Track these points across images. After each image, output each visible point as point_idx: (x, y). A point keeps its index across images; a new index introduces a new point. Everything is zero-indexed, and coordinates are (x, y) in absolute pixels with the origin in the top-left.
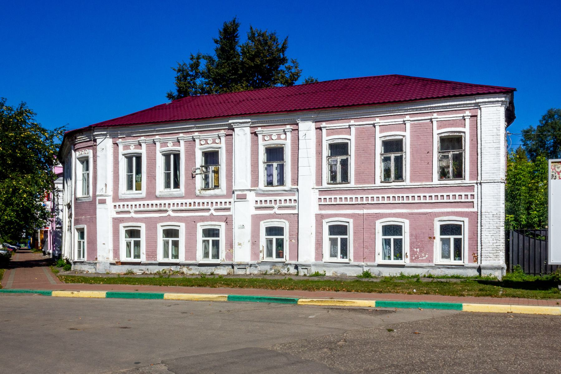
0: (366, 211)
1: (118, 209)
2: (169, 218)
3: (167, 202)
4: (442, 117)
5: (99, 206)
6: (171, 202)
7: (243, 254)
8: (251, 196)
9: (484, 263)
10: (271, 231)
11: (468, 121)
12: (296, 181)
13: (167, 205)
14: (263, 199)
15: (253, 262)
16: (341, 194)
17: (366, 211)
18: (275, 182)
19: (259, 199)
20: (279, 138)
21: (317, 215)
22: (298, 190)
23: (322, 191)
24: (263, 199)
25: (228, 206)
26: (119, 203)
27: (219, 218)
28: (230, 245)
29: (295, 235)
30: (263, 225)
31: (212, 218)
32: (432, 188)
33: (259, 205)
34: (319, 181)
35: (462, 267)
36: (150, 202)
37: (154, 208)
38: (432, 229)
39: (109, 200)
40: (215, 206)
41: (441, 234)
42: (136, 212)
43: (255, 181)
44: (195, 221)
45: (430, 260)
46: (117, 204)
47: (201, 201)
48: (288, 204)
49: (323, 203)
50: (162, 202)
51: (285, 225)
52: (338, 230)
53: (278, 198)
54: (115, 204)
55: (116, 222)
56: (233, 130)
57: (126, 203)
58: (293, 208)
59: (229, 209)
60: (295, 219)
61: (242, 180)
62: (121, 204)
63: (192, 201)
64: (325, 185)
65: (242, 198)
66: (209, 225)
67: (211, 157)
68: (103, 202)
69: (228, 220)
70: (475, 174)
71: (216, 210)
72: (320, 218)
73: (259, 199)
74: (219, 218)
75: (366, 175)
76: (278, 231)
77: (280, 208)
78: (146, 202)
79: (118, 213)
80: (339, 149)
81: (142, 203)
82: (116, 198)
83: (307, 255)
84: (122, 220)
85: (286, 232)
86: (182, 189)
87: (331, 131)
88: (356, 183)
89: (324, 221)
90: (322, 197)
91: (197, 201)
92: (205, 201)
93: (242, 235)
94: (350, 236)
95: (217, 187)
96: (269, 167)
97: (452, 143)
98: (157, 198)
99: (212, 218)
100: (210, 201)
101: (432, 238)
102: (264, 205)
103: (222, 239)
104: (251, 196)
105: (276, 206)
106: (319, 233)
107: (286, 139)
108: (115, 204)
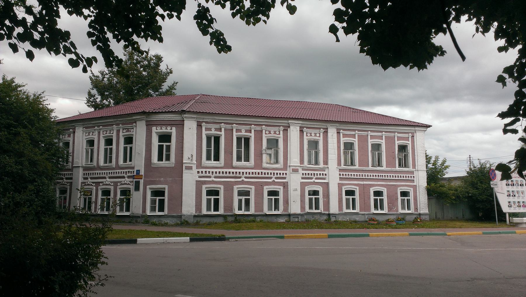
0: (365, 183)
1: (200, 174)
2: (243, 182)
3: (241, 171)
4: (400, 135)
5: (184, 171)
6: (245, 171)
7: (295, 208)
8: (301, 171)
9: (422, 212)
10: (210, 193)
11: (410, 138)
12: (326, 162)
13: (241, 173)
14: (307, 172)
15: (302, 213)
16: (346, 172)
17: (365, 183)
18: (313, 162)
19: (304, 172)
20: (315, 136)
21: (197, 181)
22: (328, 167)
23: (340, 170)
24: (307, 172)
25: (284, 176)
26: (202, 170)
27: (279, 184)
28: (286, 202)
29: (327, 196)
30: (204, 189)
31: (274, 183)
32: (396, 172)
33: (304, 176)
34: (339, 164)
35: (357, 214)
36: (228, 170)
37: (231, 175)
38: (397, 193)
39: (194, 167)
40: (276, 176)
41: (207, 196)
42: (215, 177)
43: (302, 161)
44: (262, 185)
45: (397, 211)
46: (200, 170)
47: (266, 171)
48: (321, 176)
49: (341, 177)
50: (238, 171)
51: (320, 189)
52: (350, 193)
53: (316, 172)
54: (198, 170)
55: (199, 184)
56: (289, 127)
57: (208, 170)
58: (324, 179)
59: (285, 178)
60: (326, 186)
61: (294, 160)
62: (204, 170)
63: (260, 171)
64: (343, 167)
65: (295, 171)
66: (273, 188)
67: (273, 143)
68: (190, 168)
69: (285, 186)
70: (414, 166)
71: (276, 178)
72: (340, 186)
73: (304, 172)
74: (279, 184)
75: (363, 162)
76: (316, 193)
77: (316, 179)
78: (254, 171)
79: (200, 177)
80: (349, 146)
81: (221, 170)
82: (199, 165)
83: (334, 209)
84: (205, 183)
85: (321, 193)
86: (252, 162)
87: (345, 136)
88: (359, 166)
89: (204, 187)
90: (341, 173)
91: (264, 171)
92: (269, 171)
93: (295, 195)
94: (357, 197)
95: (277, 162)
96: (345, 153)
97: (403, 148)
98: (233, 168)
99: (274, 183)
100: (272, 172)
101: (397, 199)
102: (307, 176)
103: (281, 197)
104: (301, 171)
105: (315, 177)
106: (340, 195)
107: (320, 136)
108: (198, 170)
